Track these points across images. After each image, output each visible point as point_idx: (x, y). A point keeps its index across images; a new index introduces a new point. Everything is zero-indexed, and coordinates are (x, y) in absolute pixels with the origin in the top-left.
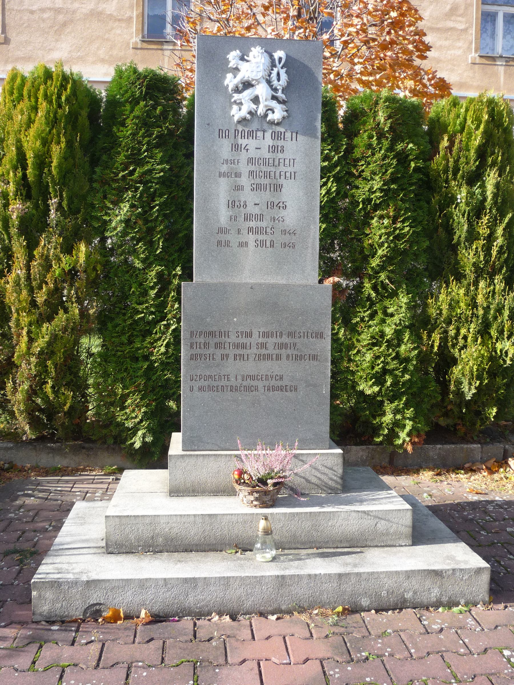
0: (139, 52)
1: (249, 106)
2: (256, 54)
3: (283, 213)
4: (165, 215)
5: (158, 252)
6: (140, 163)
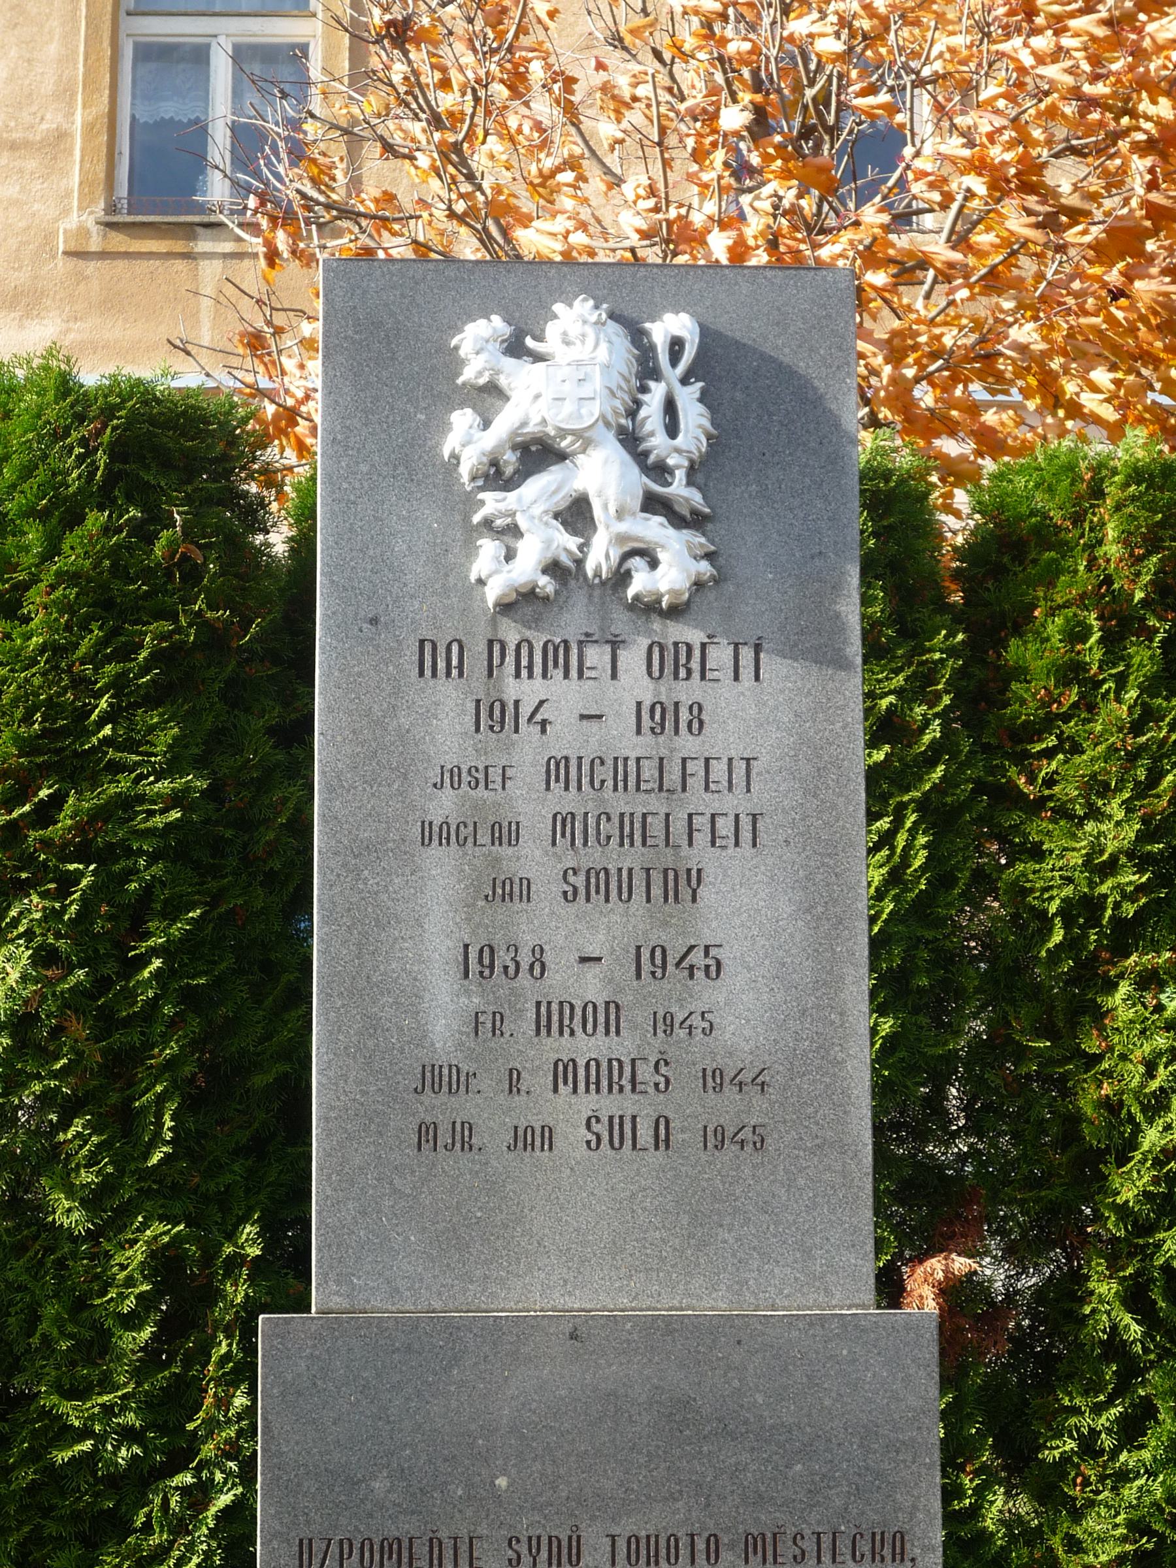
0: (91, 267)
1: (548, 543)
2: (575, 330)
3: (707, 994)
4: (189, 997)
5: (155, 1159)
6: (80, 770)
